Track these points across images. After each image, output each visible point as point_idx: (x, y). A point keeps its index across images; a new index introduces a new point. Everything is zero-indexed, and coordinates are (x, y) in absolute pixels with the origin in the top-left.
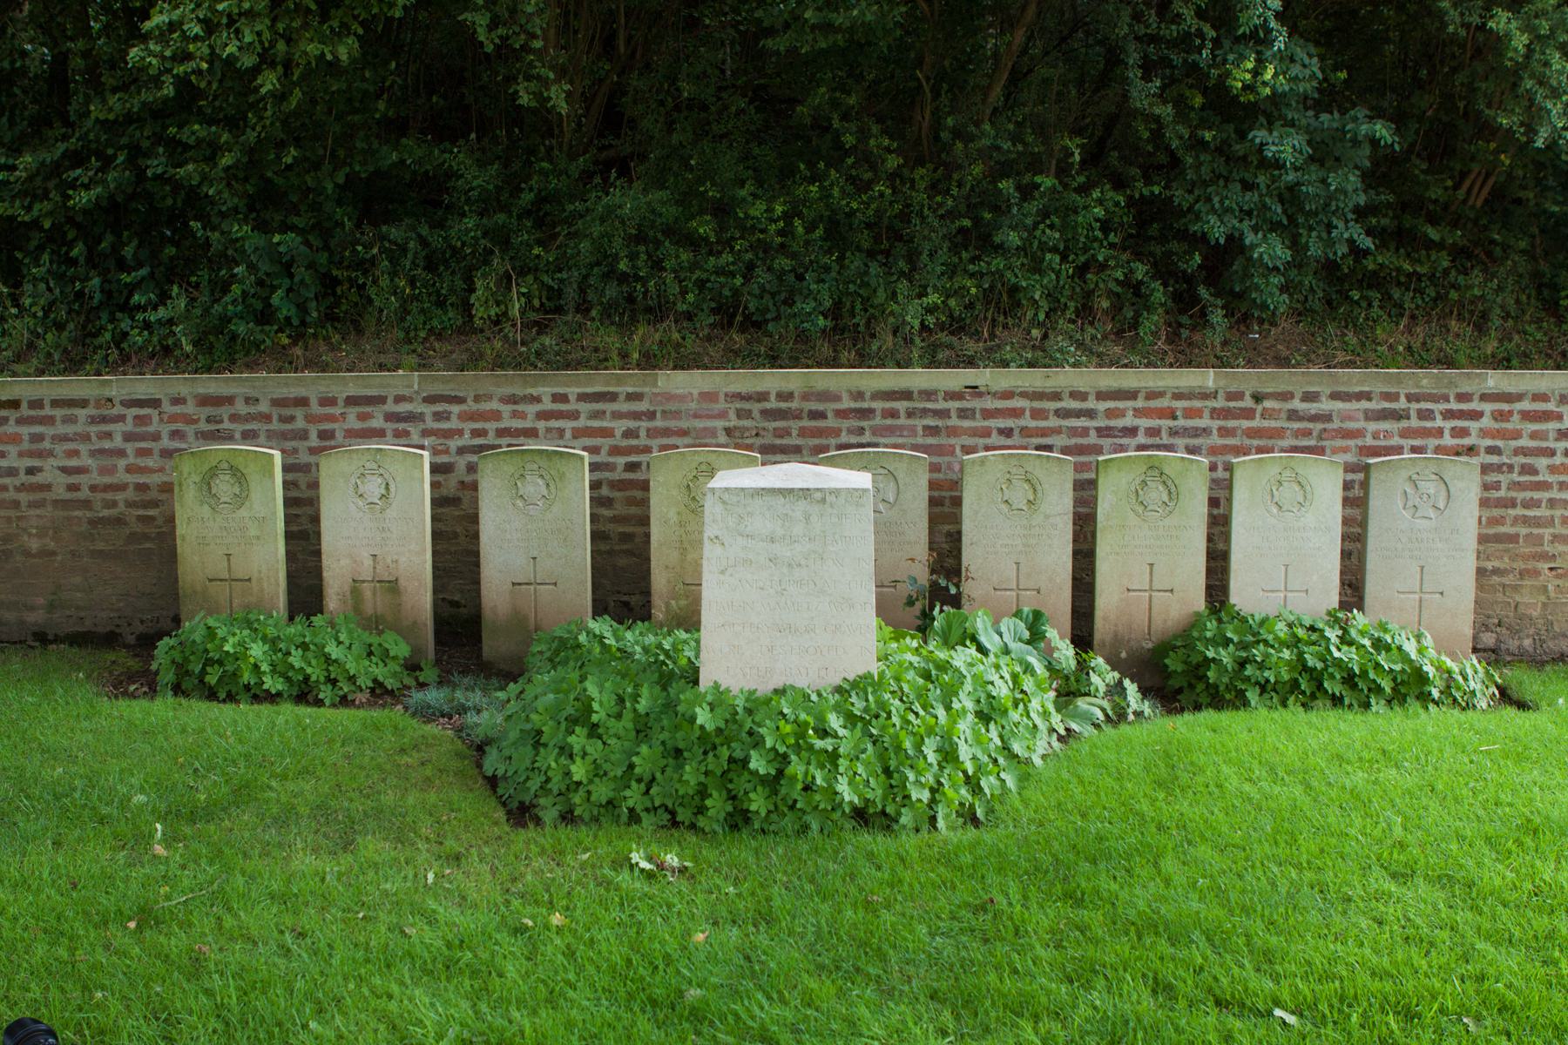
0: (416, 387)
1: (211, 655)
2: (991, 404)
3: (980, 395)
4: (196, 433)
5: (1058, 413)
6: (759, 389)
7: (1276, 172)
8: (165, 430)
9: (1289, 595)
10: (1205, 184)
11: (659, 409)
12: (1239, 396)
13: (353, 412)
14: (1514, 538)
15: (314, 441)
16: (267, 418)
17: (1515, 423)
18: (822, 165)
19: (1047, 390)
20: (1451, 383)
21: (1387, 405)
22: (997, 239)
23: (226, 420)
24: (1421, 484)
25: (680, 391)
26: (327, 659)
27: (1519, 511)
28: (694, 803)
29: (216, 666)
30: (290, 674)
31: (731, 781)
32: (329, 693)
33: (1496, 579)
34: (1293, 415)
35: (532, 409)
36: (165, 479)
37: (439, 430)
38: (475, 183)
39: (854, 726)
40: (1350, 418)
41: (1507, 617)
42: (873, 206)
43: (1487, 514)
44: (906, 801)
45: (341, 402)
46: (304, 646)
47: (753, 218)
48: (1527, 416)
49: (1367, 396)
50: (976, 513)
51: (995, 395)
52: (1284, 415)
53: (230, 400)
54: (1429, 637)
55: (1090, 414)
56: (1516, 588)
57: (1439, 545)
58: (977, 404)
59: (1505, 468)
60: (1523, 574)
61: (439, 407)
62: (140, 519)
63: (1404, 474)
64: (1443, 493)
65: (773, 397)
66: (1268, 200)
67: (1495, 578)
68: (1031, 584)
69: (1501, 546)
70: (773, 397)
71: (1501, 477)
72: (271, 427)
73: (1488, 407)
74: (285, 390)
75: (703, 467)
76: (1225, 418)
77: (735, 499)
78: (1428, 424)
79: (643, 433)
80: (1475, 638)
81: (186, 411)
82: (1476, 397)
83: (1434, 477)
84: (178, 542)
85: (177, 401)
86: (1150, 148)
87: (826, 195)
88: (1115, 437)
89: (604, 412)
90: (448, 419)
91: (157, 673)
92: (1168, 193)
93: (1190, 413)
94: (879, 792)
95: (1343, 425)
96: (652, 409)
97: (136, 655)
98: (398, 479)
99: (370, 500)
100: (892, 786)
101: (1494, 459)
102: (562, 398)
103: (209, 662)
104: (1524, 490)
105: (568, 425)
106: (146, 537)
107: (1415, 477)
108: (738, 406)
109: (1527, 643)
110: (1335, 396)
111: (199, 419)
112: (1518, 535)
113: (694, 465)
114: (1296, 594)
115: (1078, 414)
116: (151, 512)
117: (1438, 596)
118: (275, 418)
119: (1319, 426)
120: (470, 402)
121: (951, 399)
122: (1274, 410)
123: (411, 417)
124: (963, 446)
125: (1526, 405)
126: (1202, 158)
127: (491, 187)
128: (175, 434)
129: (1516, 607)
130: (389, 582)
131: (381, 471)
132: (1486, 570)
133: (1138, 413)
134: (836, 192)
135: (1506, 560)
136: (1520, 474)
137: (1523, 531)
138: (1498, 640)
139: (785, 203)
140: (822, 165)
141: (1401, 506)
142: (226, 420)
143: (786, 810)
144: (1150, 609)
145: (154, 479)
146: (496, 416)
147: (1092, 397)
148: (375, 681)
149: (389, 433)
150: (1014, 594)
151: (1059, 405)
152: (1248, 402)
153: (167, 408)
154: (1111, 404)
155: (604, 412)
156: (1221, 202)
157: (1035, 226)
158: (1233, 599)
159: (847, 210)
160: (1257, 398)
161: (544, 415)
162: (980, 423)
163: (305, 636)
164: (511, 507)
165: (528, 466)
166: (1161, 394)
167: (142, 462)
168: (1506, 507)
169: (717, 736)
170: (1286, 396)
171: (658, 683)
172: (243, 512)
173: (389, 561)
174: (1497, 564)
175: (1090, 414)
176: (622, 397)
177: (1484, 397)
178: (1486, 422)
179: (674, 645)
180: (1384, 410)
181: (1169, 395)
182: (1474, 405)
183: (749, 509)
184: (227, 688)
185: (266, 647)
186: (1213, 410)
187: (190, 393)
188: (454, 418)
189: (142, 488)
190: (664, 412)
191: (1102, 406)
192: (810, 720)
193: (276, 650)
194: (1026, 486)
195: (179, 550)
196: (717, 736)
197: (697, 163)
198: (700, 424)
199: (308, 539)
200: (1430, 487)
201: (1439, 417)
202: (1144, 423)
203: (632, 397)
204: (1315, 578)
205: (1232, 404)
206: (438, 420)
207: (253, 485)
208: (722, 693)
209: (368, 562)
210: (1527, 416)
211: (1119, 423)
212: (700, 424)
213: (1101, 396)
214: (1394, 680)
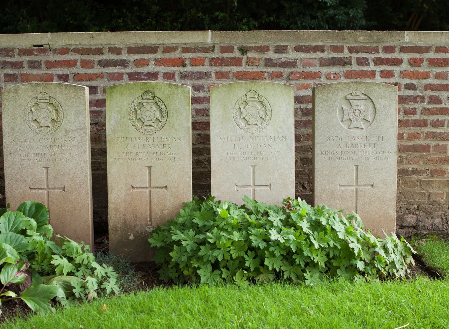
2: (52, 57)
3: (45, 51)
5: (100, 63)
7: (325, 11)
9: (257, 189)
12: (230, 49)
14: (426, 148)
17: (424, 68)
19: (93, 47)
20: (380, 40)
21: (335, 55)
24: (354, 103)
27: (429, 129)
33: (414, 177)
34: (269, 63)
40: (310, 65)
41: (423, 203)
43: (406, 131)
48: (433, 62)
49: (321, 49)
50: (13, 129)
51: (55, 51)
52: (262, 63)
54: (359, 218)
55: (124, 63)
56: (428, 183)
57: (370, 149)
58: (42, 58)
59: (418, 99)
60: (433, 173)
63: (341, 95)
64: (371, 109)
66: (322, 23)
67: (414, 176)
68: (59, 185)
69: (418, 154)
71: (416, 106)
73: (405, 56)
76: (220, 65)
78: (365, 68)
80: (399, 219)
82: (397, 49)
83: (363, 97)
88: (142, 79)
93: (195, 62)
95: (305, 70)
101: (411, 93)
104: (432, 114)
107: (349, 97)
109: (437, 221)
110: (298, 49)
112: (429, 146)
114: (262, 188)
115: (115, 64)
117: (370, 187)
119: (288, 70)
121: (24, 54)
122: (255, 59)
125: (432, 55)
126: (293, 4)
129: (429, 196)
132: (408, 171)
133: (158, 62)
135: (421, 163)
136: (429, 103)
137: (433, 143)
138: (417, 220)
141: (339, 120)
144: (150, 202)
147: (124, 52)
151: (101, 57)
152: (236, 54)
154: (138, 56)
156: (301, 24)
158: (213, 194)
160: (243, 51)
162: (44, 71)
166: (173, 49)
168: (420, 126)
170: (264, 49)
174: (415, 166)
175: (124, 63)
177: (403, 50)
178: (405, 67)
180: (333, 58)
181: (180, 49)
182: (396, 55)
186: (212, 60)
191: (132, 58)
194: (50, 108)
200: (361, 105)
201: (372, 63)
202: (162, 69)
204: (276, 175)
205: (225, 55)
210: (433, 62)
211: (145, 70)
213: (131, 50)
214: (327, 255)
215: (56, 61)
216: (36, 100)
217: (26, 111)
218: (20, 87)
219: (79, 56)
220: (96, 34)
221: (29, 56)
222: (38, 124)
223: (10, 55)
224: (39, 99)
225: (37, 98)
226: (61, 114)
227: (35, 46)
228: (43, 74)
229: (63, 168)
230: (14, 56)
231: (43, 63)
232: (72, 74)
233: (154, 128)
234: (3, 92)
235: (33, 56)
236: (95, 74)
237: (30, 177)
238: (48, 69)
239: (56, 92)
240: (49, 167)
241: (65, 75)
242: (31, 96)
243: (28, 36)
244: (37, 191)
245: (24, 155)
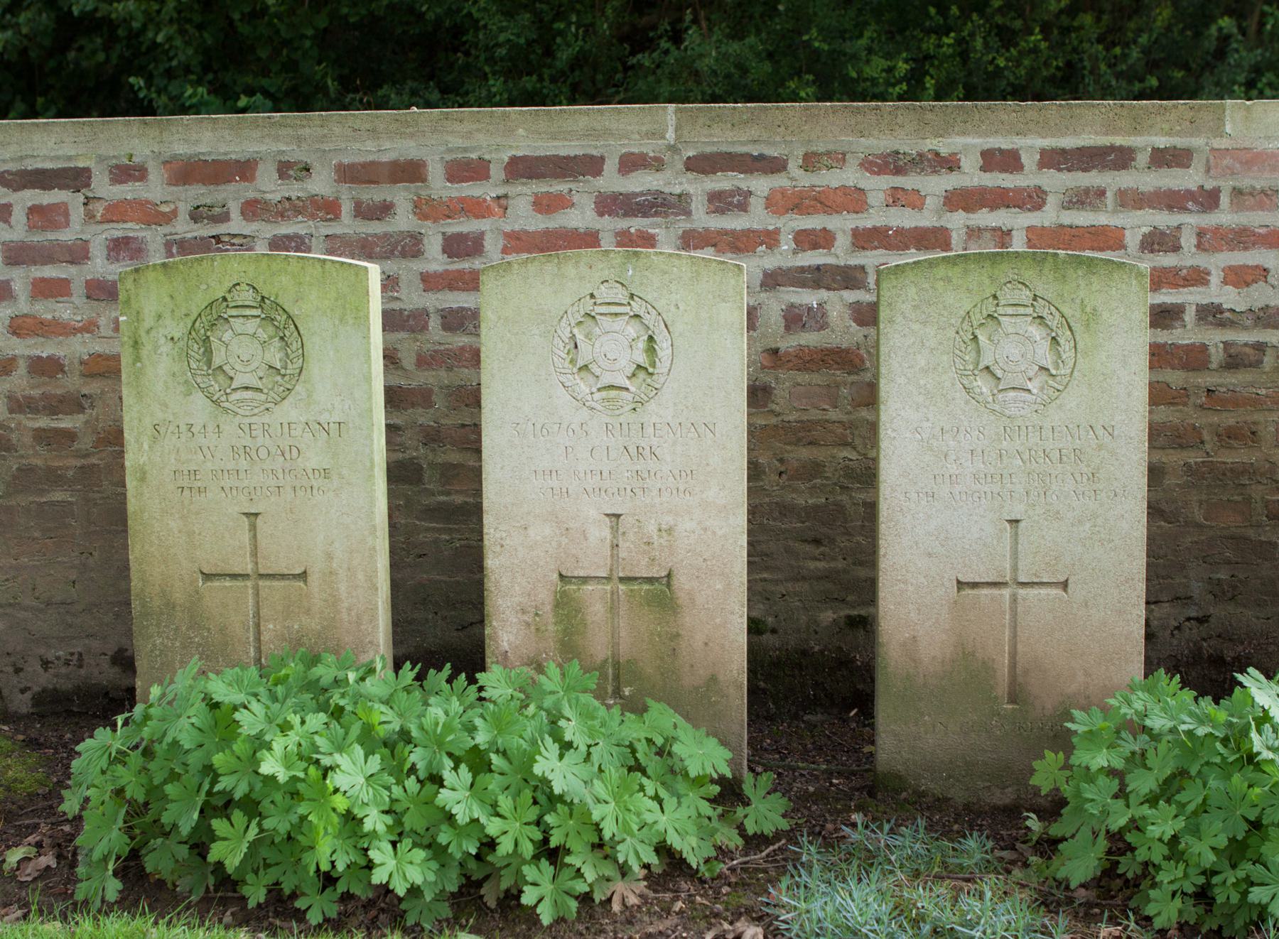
0: (670, 135)
1: (224, 784)
4: (168, 245)
8: (98, 238)
11: (1226, 185)
13: (524, 193)
15: (435, 260)
16: (329, 209)
18: (954, 10)
23: (235, 214)
26: (545, 797)
29: (238, 816)
30: (443, 839)
32: (547, 888)
35: (935, 185)
36: (98, 347)
37: (725, 232)
38: (502, 38)
42: (1026, 62)
45: (497, 172)
46: (478, 762)
53: (244, 169)
61: (724, 182)
62: (43, 437)
72: (335, 229)
74: (370, 145)
79: (1188, 240)
81: (145, 195)
84: (131, 483)
85: (127, 172)
87: (963, 52)
89: (1101, 193)
90: (743, 207)
91: (79, 754)
97: (33, 744)
98: (677, 328)
99: (606, 379)
102: (1006, 161)
103: (221, 806)
105: (1018, 221)
106: (54, 478)
111: (174, 213)
116: (65, 423)
118: (347, 208)
120: (793, 167)
123: (656, 205)
127: (522, 41)
128: (120, 247)
130: (650, 580)
131: (637, 307)
134: (979, 43)
139: (906, 61)
142: (235, 214)
145: (75, 349)
146: (854, 200)
148: (663, 849)
149: (607, 242)
153: (103, 187)
155: (1101, 193)
159: (990, 68)
161: (961, 200)
163: (471, 729)
164: (960, 395)
165: (1007, 295)
167: (47, 310)
172: (289, 411)
173: (651, 528)
176: (1142, 159)
184: (268, 877)
185: (375, 763)
187: (156, 155)
188: (757, 204)
189: (46, 368)
190: (1237, 192)
193: (403, 772)
195: (132, 505)
197: (787, 10)
199: (419, 480)
203: (1165, 158)
206: (720, 211)
207: (314, 344)
209: (600, 533)
224: (1002, 302)
233: (263, 397)
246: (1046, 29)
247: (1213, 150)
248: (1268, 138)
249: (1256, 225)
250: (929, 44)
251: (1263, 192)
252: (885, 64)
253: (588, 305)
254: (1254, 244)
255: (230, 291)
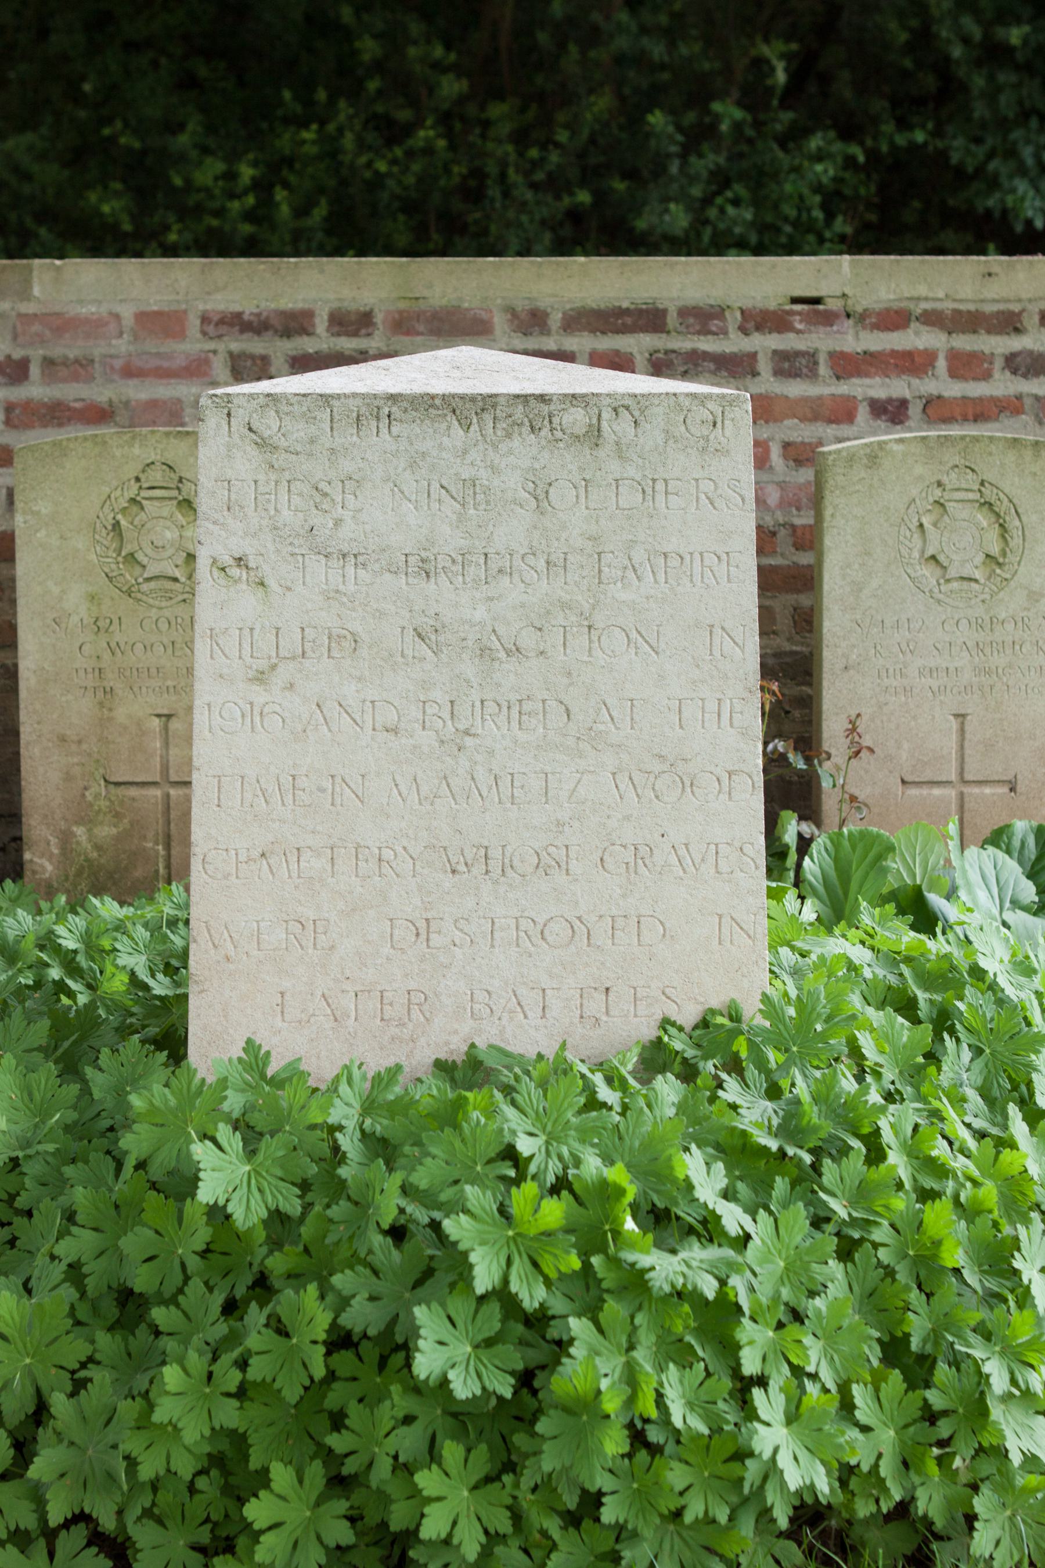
3: (828, 319)
5: (1013, 363)
6: (286, 304)
10: (1003, 125)
11: (36, 354)
18: (322, 95)
19: (989, 308)
22: (641, 224)
25: (88, 310)
28: (197, 1508)
31: (338, 1421)
39: (763, 1186)
42: (416, 167)
44: (987, 1467)
47: (199, 190)
51: (863, 319)
65: (321, 325)
70: (321, 325)
75: (156, 476)
77: (299, 431)
86: (908, 63)
87: (331, 152)
92: (940, 144)
94: (887, 1437)
96: (17, 354)
100: (931, 1417)
108: (235, 346)
113: (131, 470)
121: (759, 328)
124: (787, 446)
134: (348, 141)
139: (255, 164)
140: (322, 95)
143: (553, 1526)
150: (951, 793)
157: (707, 201)
159: (368, 174)
169: (275, 1244)
171: (46, 1051)
179: (88, 939)
183: (347, 466)
190: (49, 363)
192: (618, 1174)
194: (983, 519)
196: (275, 1244)
198: (139, 392)
208: (278, 1083)
212: (139, 392)
215: (865, 353)
216: (938, 492)
217: (903, 527)
218: (888, 447)
219: (943, 337)
220: (1001, 263)
221: (775, 335)
222: (939, 571)
223: (714, 329)
224: (948, 487)
225: (939, 484)
226: (1015, 542)
227: (795, 300)
228: (820, 398)
229: (1015, 715)
230: (725, 333)
231: (822, 359)
232: (920, 397)
234: (830, 462)
235: (792, 335)
236: (994, 400)
237: (906, 746)
238: (838, 378)
239: (1002, 465)
240: (969, 711)
241: (897, 400)
242: (921, 478)
243: (774, 266)
244: (925, 791)
245: (891, 671)
246: (445, 119)
247: (20, 315)
248: (80, 302)
249: (71, 398)
250: (284, 142)
251: (77, 361)
252: (220, 167)
253: (132, 491)
254: (69, 420)
255: (143, 471)
